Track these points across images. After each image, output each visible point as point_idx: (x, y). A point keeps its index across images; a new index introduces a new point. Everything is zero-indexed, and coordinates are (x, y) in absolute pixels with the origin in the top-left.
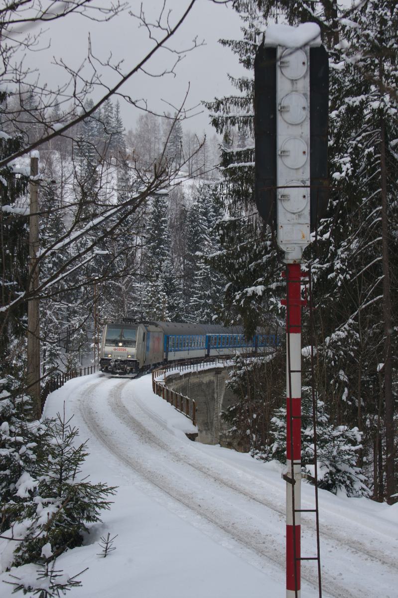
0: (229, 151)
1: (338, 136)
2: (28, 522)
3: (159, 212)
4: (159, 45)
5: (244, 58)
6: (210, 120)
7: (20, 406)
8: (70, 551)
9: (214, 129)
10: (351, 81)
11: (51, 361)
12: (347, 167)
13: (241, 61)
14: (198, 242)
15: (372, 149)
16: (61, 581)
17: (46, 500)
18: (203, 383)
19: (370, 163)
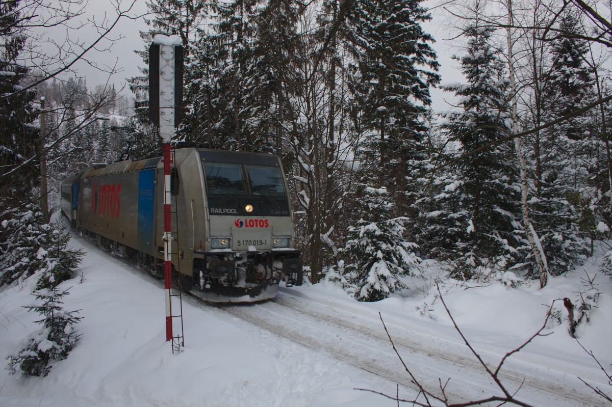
0: (138, 101)
1: (188, 96)
2: (43, 270)
4: (102, 36)
5: (145, 59)
6: (129, 87)
7: (38, 217)
8: (64, 282)
9: (131, 91)
10: (194, 72)
11: (53, 200)
12: (192, 110)
13: (144, 61)
15: (203, 103)
16: (60, 292)
17: (52, 259)
19: (202, 108)
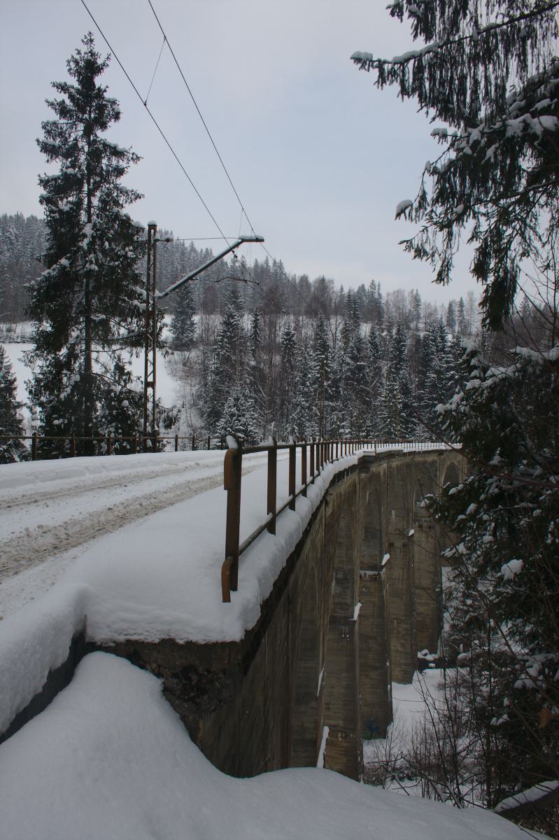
3: (400, 338)
14: (429, 361)
18: (427, 462)
